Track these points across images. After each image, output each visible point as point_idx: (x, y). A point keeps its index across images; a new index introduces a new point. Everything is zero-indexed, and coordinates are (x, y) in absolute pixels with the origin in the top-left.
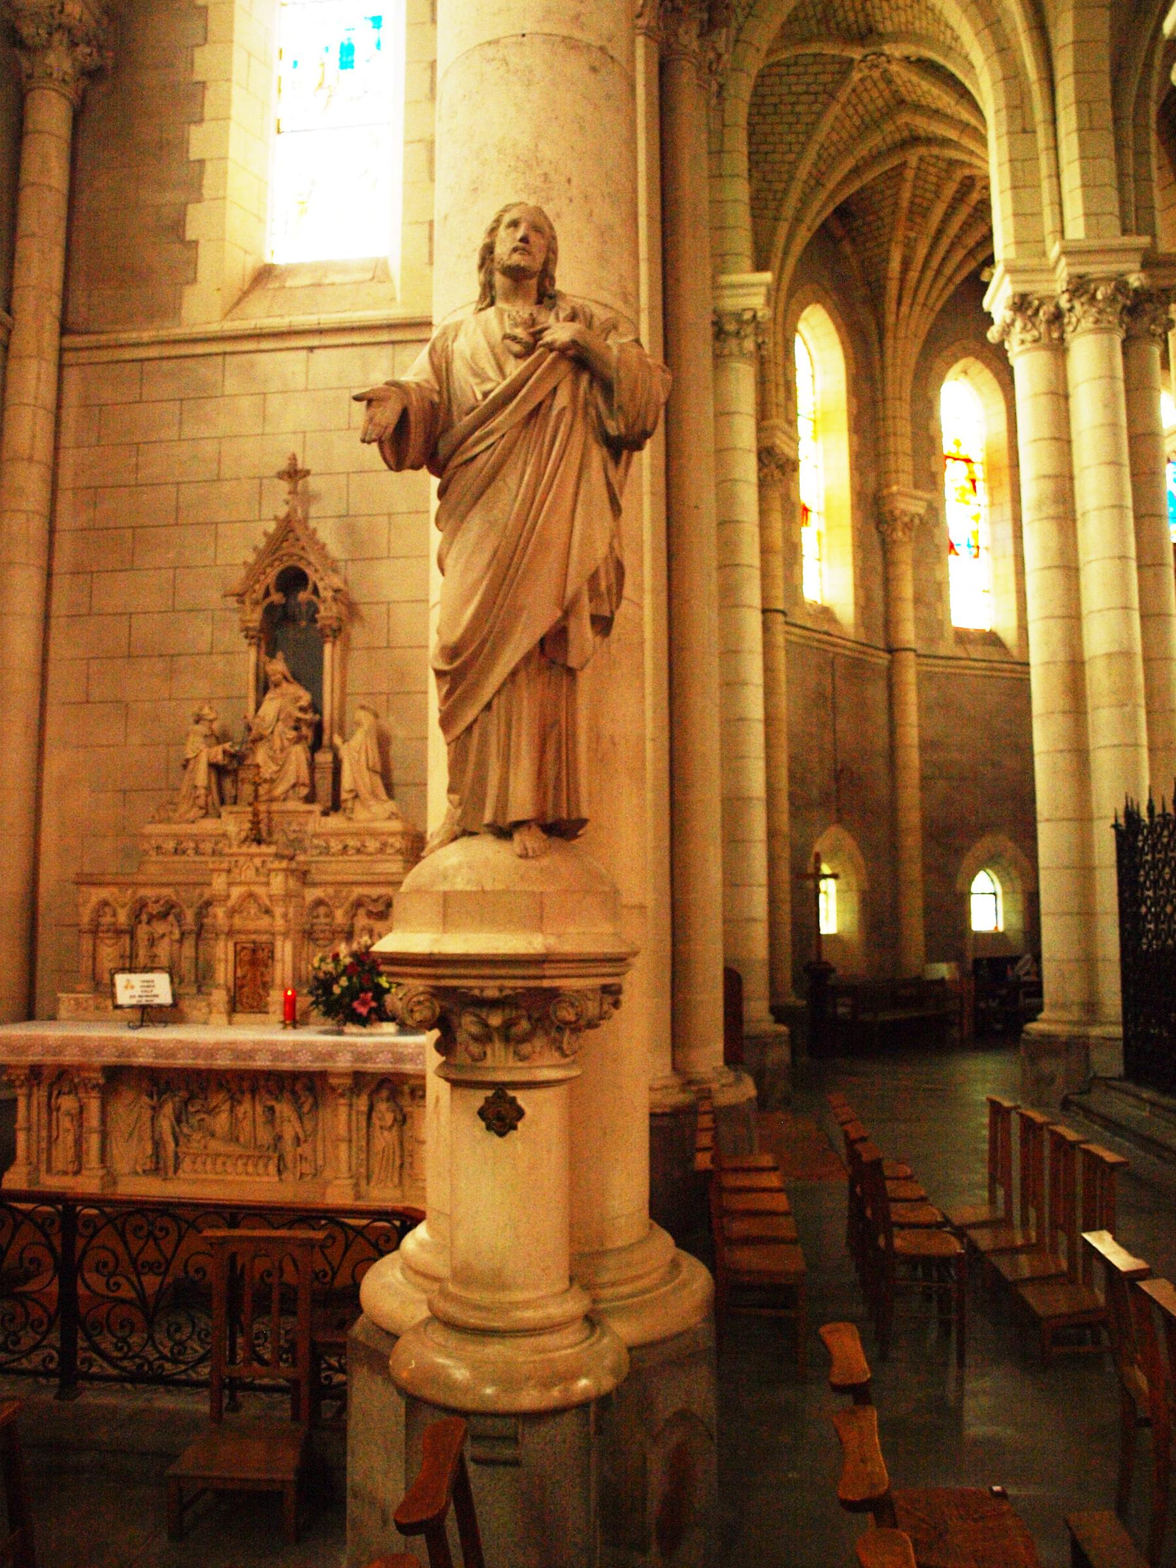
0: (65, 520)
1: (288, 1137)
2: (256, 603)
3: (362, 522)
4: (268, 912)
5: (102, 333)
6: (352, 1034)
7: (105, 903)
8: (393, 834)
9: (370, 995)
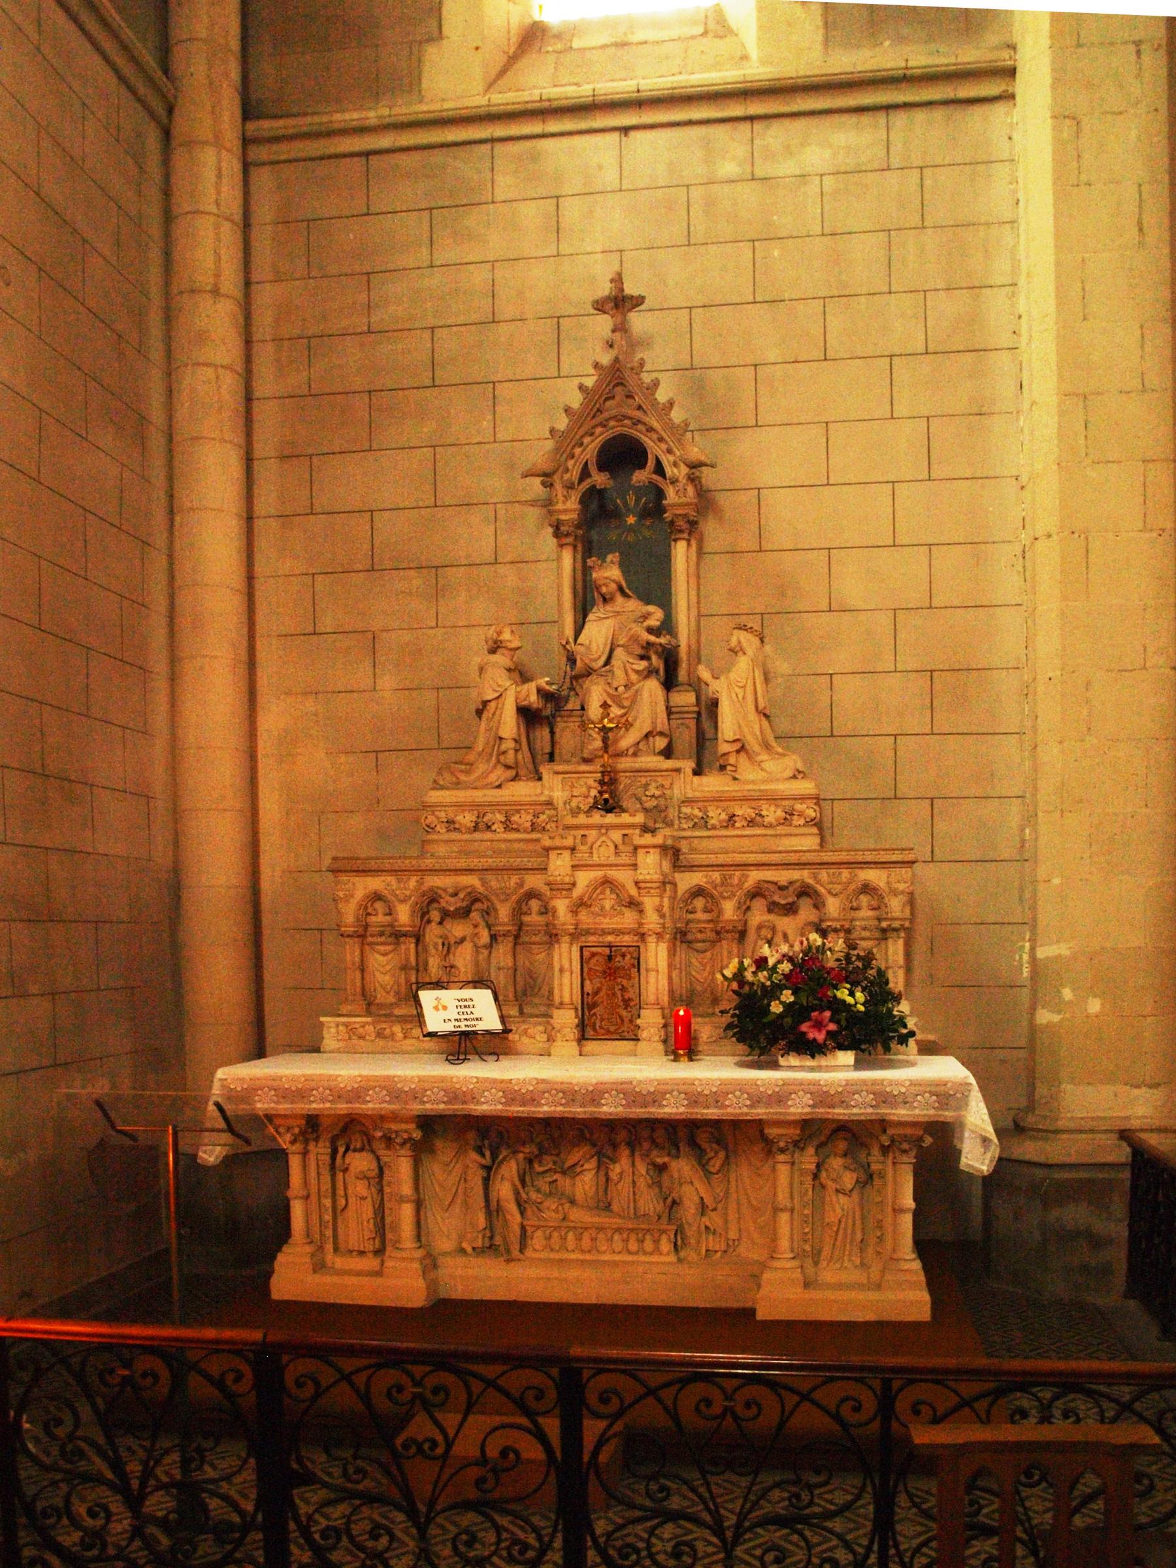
0: (265, 385)
1: (690, 1208)
2: (570, 487)
3: (715, 376)
4: (633, 904)
5: (305, 114)
6: (791, 1068)
7: (377, 897)
8: (802, 798)
9: (828, 1014)
